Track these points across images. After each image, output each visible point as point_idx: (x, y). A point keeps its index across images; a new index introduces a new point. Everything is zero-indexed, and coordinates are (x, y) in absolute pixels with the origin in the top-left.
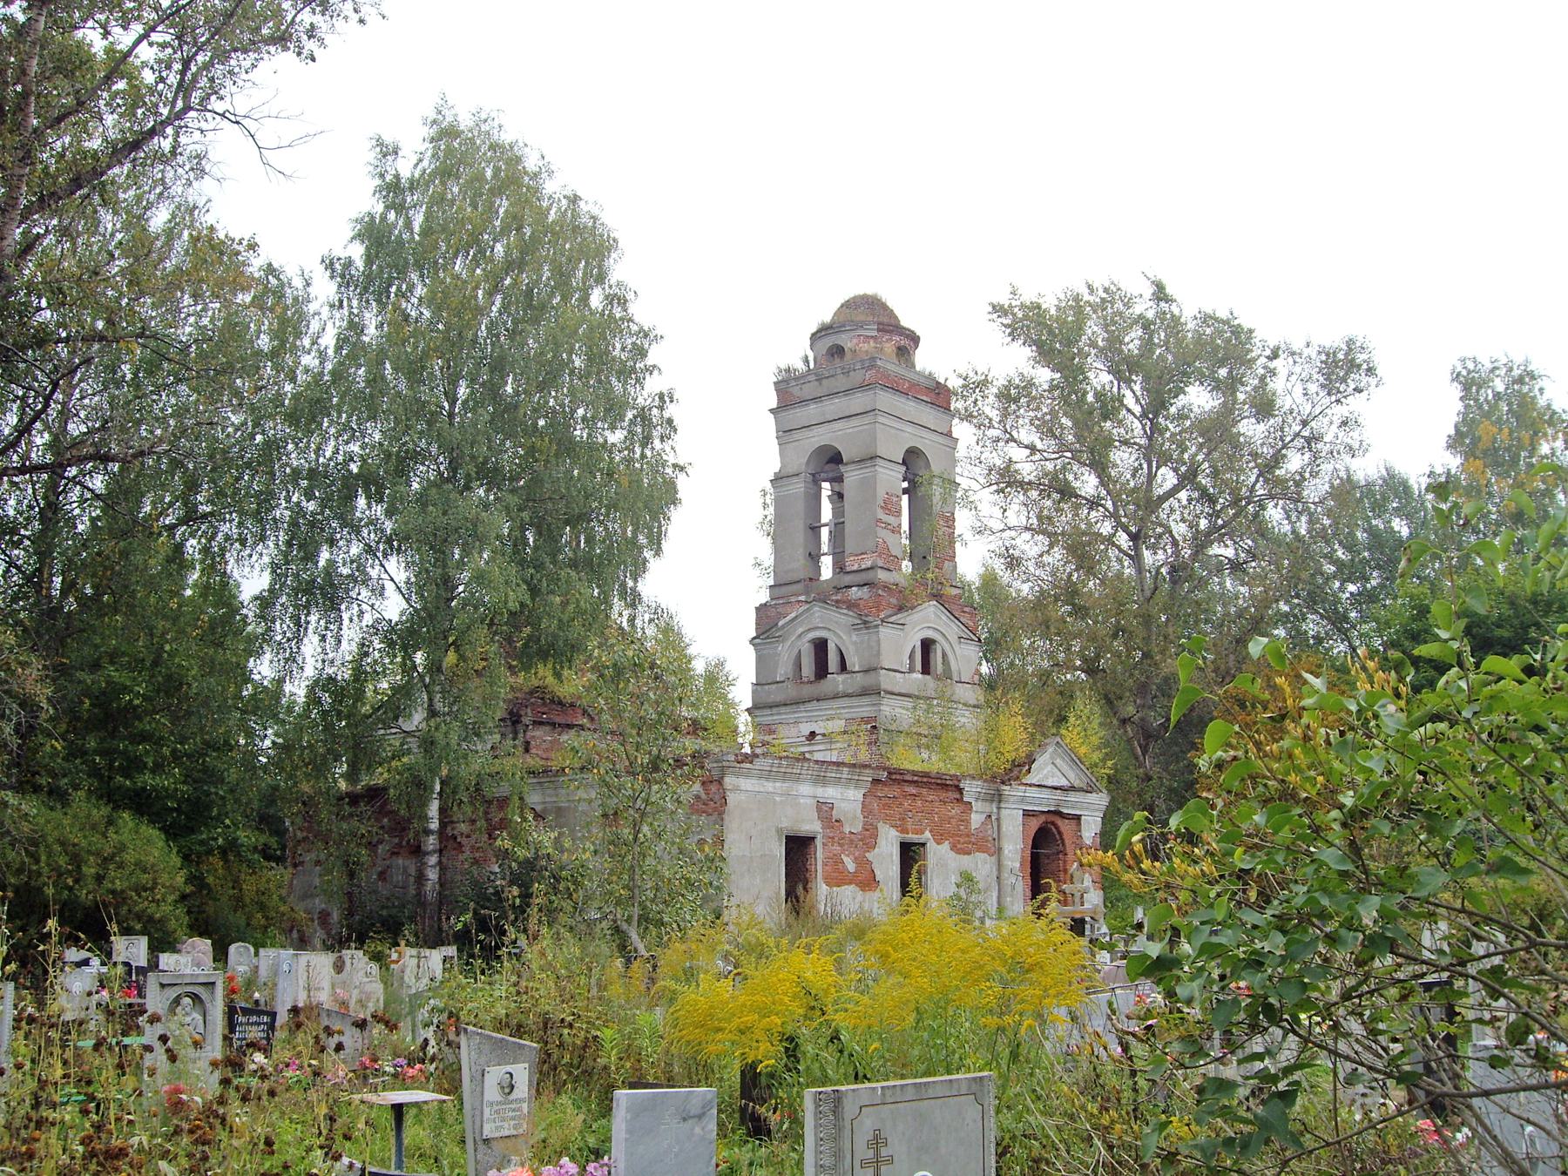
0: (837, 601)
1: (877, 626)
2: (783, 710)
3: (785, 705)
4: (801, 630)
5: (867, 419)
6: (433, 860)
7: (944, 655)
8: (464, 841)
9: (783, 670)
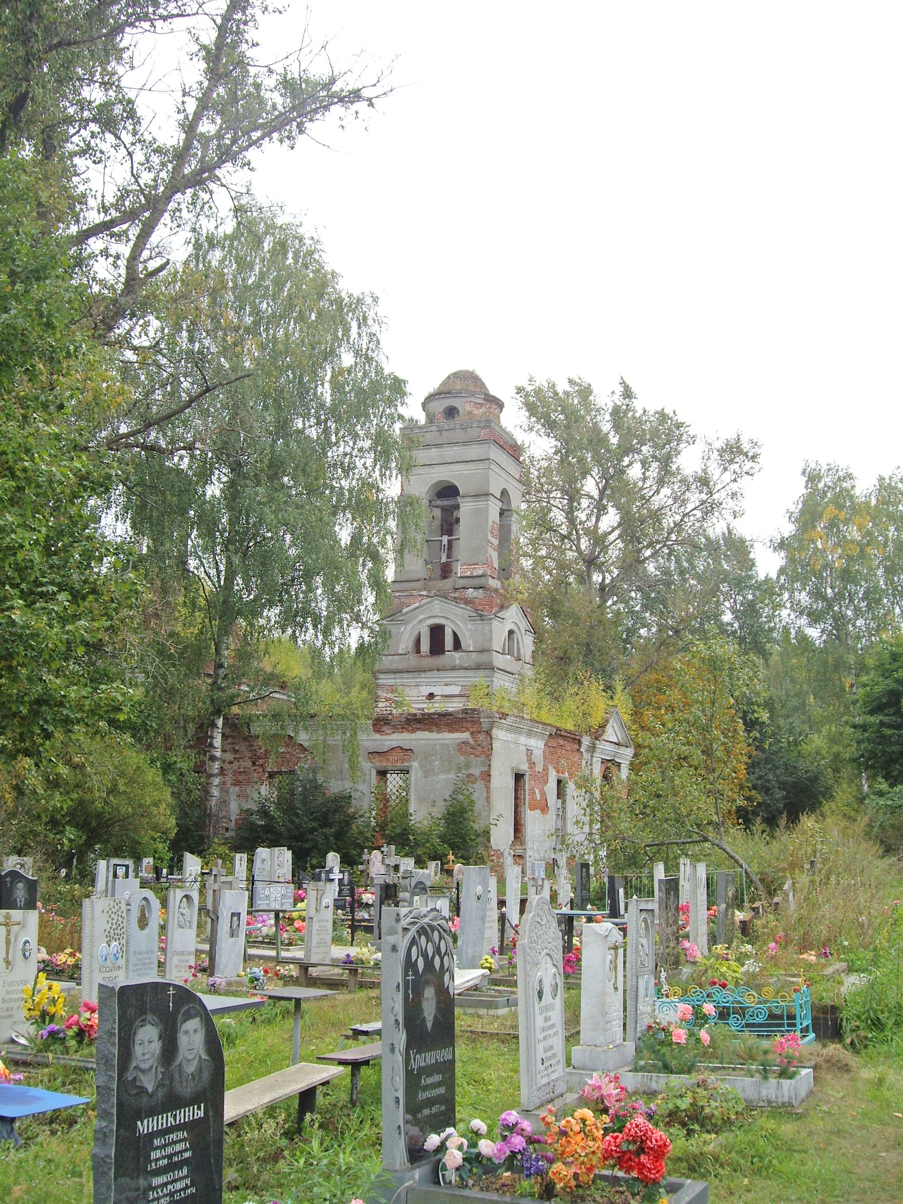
0: (455, 598)
1: (491, 619)
2: (405, 675)
3: (408, 672)
4: (422, 617)
5: (481, 465)
7: (518, 642)
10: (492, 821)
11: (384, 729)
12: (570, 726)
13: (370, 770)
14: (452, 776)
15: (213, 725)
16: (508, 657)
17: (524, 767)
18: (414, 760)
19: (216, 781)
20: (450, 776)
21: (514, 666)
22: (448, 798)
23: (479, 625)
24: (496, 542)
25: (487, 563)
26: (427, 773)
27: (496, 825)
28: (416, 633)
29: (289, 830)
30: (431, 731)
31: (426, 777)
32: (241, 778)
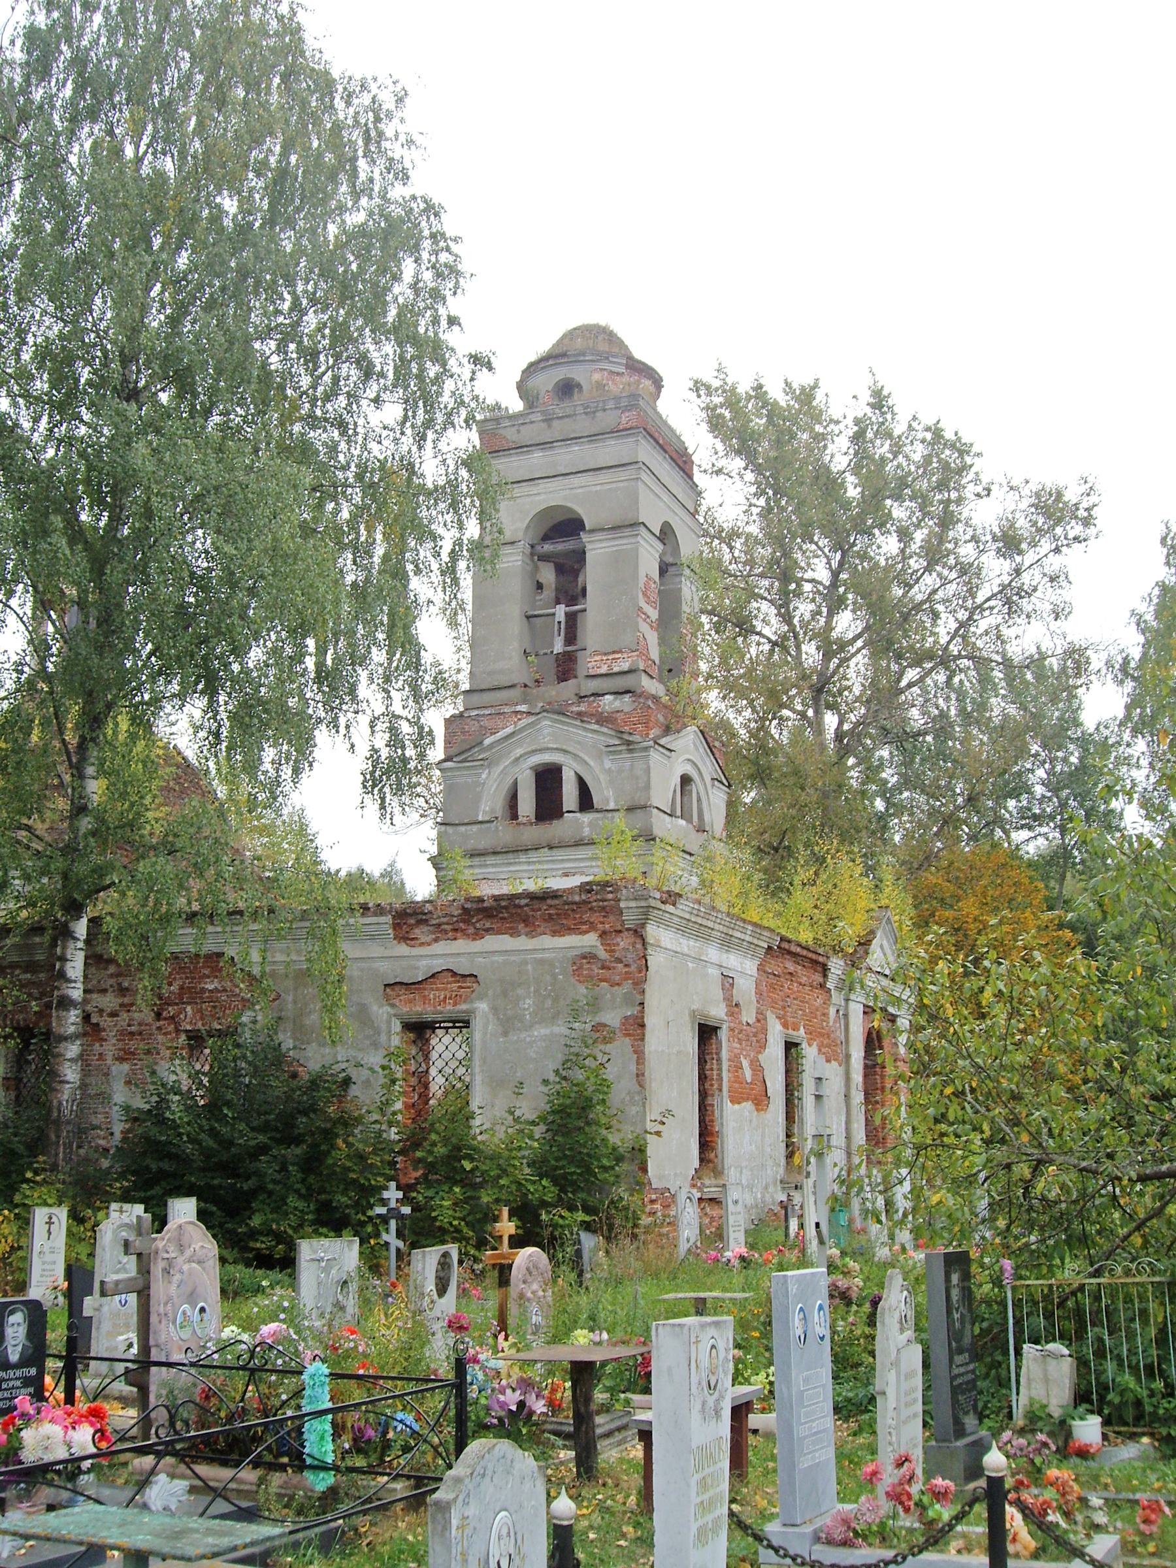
0: (580, 714)
1: (646, 749)
2: (490, 860)
3: (495, 853)
4: (519, 752)
5: (623, 474)
6: (73, 1050)
7: (699, 800)
8: (105, 1022)
9: (491, 803)
10: (650, 1126)
11: (417, 932)
12: (805, 936)
13: (389, 1022)
14: (560, 1029)
15: (65, 933)
16: (682, 822)
17: (717, 1012)
18: (481, 998)
19: (73, 1050)
20: (556, 1030)
21: (694, 842)
22: (552, 1077)
23: (625, 761)
24: (654, 614)
25: (639, 648)
26: (508, 1024)
27: (658, 1133)
28: (509, 781)
29: (207, 1154)
30: (514, 933)
31: (505, 1033)
32: (133, 1045)
